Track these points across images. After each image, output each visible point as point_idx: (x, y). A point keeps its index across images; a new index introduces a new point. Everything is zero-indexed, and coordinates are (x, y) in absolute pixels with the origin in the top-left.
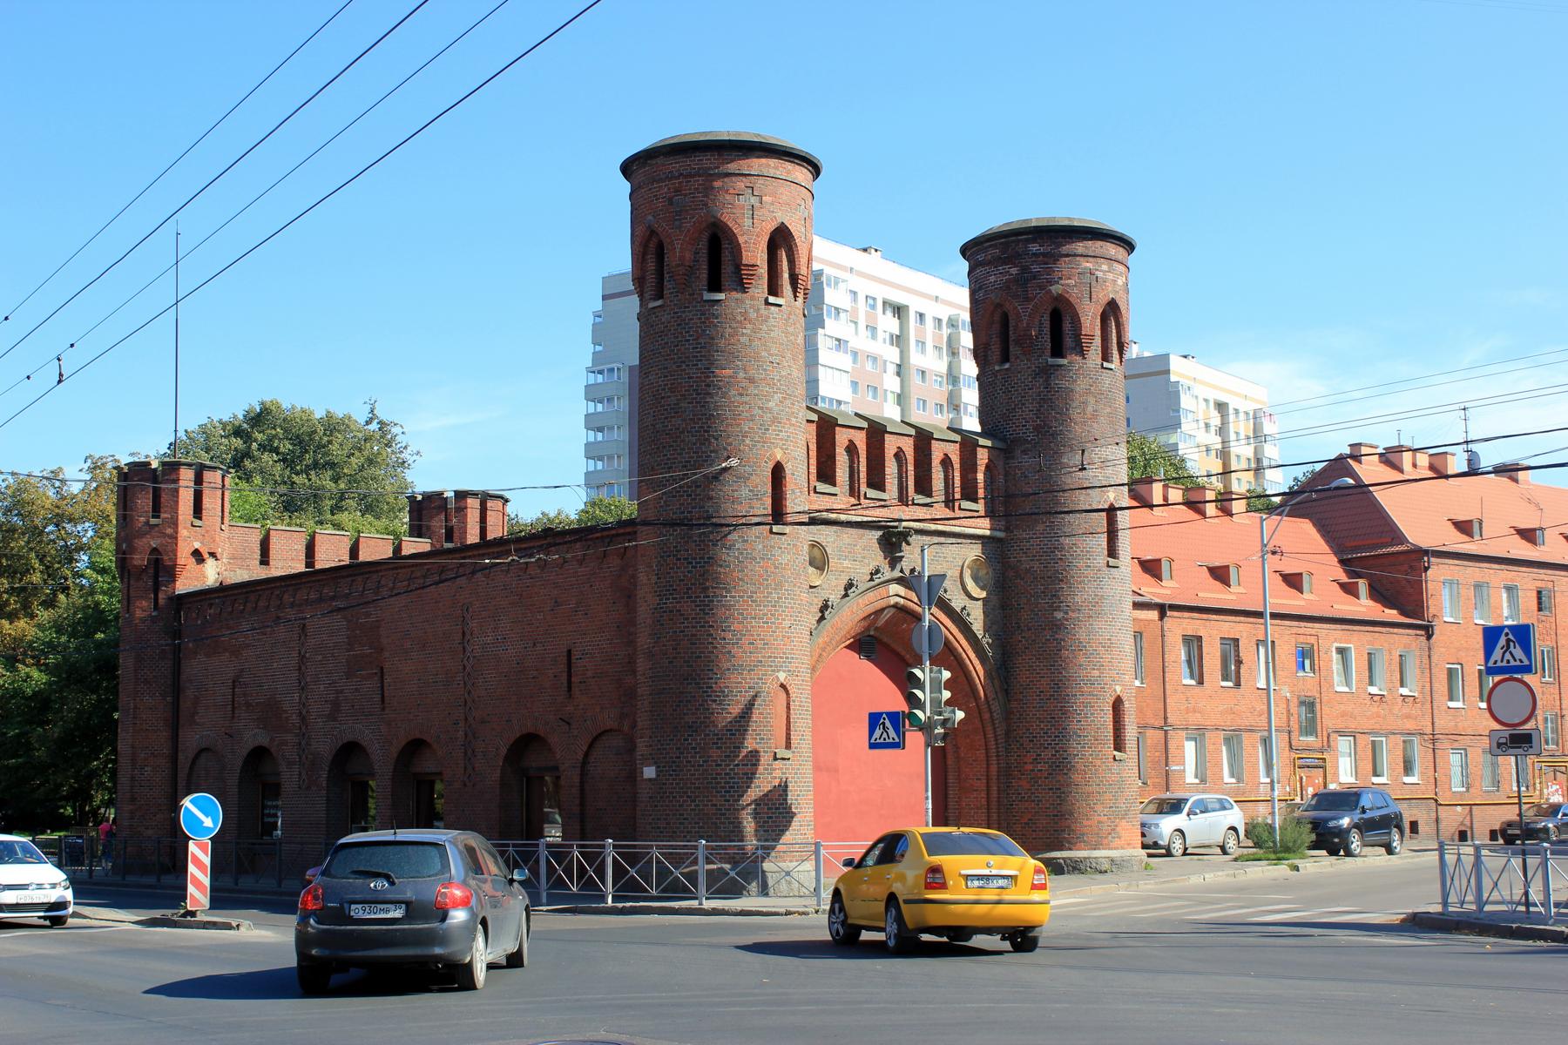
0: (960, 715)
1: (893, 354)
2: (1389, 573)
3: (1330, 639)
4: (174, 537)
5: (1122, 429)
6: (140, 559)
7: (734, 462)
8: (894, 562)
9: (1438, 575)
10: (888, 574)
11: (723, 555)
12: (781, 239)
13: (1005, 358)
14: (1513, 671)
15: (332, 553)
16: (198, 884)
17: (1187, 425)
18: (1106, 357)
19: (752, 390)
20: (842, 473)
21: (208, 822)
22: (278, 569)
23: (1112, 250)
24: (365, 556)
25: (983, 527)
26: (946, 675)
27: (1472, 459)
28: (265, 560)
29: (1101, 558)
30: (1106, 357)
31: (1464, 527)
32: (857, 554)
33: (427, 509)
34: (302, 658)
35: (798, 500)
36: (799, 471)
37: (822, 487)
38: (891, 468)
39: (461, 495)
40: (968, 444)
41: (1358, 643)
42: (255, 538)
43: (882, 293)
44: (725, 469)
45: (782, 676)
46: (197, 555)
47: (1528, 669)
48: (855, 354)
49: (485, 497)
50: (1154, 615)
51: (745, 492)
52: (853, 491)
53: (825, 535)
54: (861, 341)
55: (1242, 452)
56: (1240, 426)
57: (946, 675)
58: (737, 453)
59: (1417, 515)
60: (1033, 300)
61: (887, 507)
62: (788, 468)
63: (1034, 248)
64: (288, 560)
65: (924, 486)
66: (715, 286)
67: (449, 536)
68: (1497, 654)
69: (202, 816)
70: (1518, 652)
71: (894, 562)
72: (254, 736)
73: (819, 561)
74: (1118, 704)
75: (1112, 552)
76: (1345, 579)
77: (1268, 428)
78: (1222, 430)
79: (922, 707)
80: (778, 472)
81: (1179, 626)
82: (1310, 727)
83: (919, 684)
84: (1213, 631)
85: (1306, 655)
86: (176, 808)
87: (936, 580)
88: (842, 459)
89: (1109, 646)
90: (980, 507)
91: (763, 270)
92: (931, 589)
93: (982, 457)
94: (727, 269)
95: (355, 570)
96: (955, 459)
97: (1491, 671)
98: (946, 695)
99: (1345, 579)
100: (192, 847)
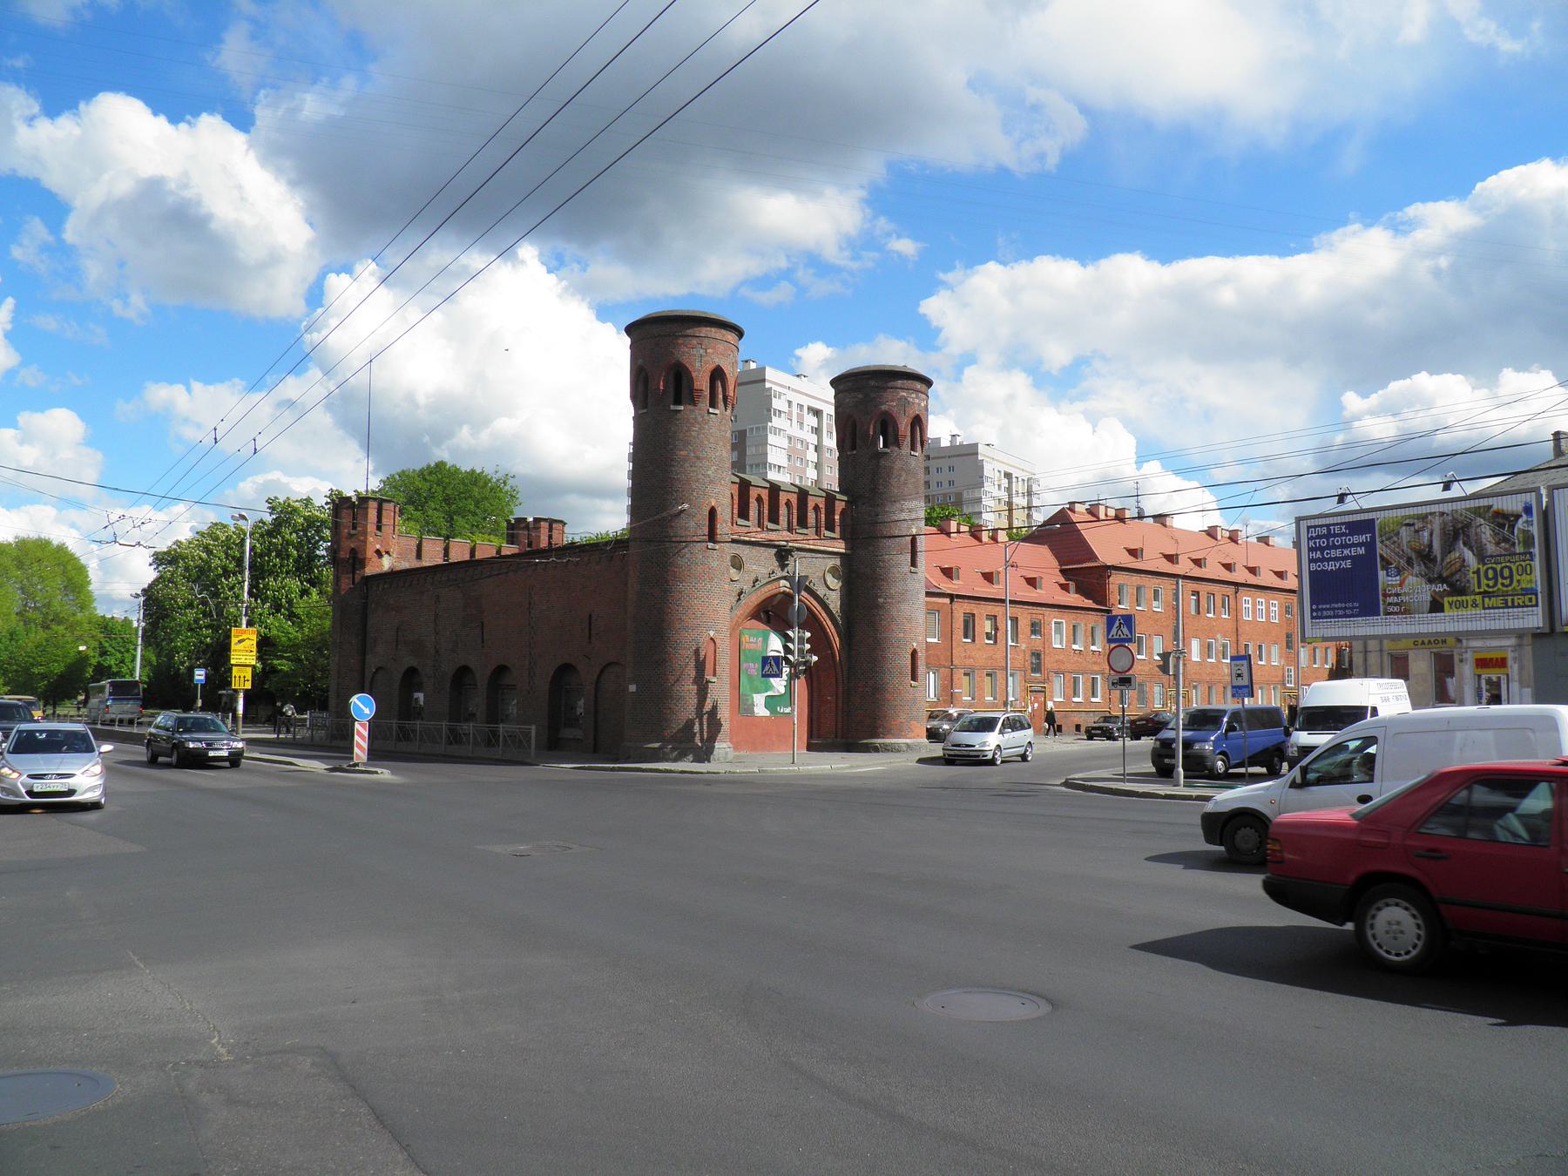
0: (815, 658)
1: (813, 439)
2: (1088, 579)
3: (1052, 619)
4: (365, 542)
5: (922, 489)
6: (344, 554)
7: (686, 506)
8: (783, 566)
9: (1116, 579)
10: (779, 574)
11: (680, 561)
12: (717, 375)
13: (854, 448)
14: (1121, 642)
15: (459, 553)
16: (359, 747)
17: (988, 486)
18: (913, 448)
19: (698, 464)
20: (753, 513)
21: (367, 711)
22: (426, 563)
23: (918, 386)
24: (478, 556)
25: (840, 547)
26: (808, 635)
27: (1140, 511)
28: (419, 556)
29: (907, 567)
30: (913, 448)
31: (1133, 553)
32: (761, 564)
33: (517, 528)
34: (437, 615)
35: (723, 528)
36: (725, 512)
37: (741, 522)
38: (783, 511)
39: (537, 520)
40: (830, 498)
41: (1065, 620)
42: (414, 543)
43: (807, 402)
44: (682, 511)
45: (712, 633)
46: (378, 553)
47: (1130, 640)
48: (790, 438)
49: (551, 522)
50: (947, 601)
51: (692, 524)
52: (760, 524)
53: (744, 552)
54: (795, 431)
55: (1020, 501)
56: (1019, 487)
57: (808, 635)
58: (689, 501)
59: (1106, 546)
60: (873, 410)
61: (781, 536)
62: (719, 510)
63: (872, 383)
64: (433, 555)
65: (803, 522)
66: (678, 402)
67: (530, 545)
68: (1114, 630)
69: (362, 707)
70: (1125, 630)
71: (783, 566)
72: (409, 661)
73: (737, 563)
74: (914, 653)
75: (914, 564)
76: (1063, 581)
77: (1035, 488)
78: (1009, 489)
79: (792, 653)
80: (713, 512)
81: (961, 609)
82: (1037, 668)
83: (792, 641)
84: (981, 610)
85: (1036, 628)
86: (346, 706)
87: (803, 578)
88: (753, 505)
89: (910, 620)
90: (837, 535)
91: (707, 393)
92: (802, 584)
93: (839, 506)
94: (685, 391)
95: (472, 564)
96: (822, 506)
97: (1110, 641)
98: (808, 646)
99: (1063, 581)
100: (357, 726)
